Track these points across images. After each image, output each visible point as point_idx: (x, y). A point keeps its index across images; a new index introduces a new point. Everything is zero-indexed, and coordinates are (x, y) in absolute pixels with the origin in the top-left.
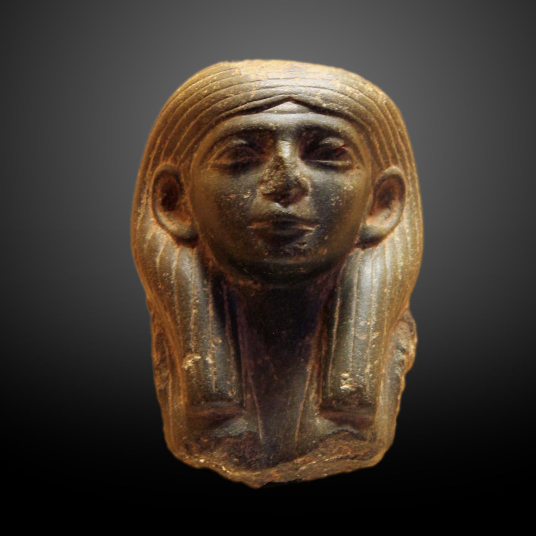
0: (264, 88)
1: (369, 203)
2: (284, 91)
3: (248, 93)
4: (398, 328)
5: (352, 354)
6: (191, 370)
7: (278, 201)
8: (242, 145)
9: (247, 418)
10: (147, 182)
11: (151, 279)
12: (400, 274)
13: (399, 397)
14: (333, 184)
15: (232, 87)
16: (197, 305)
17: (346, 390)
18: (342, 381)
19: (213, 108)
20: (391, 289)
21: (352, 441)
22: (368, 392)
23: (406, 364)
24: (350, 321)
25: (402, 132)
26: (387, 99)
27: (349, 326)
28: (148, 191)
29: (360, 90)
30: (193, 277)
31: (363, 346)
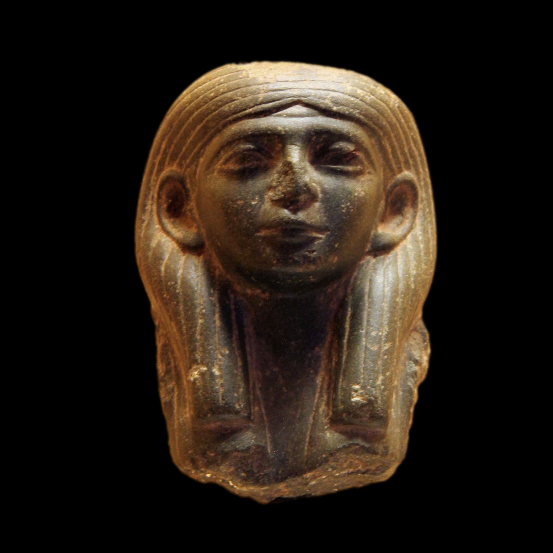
0: (273, 91)
1: (380, 209)
2: (293, 94)
3: (256, 96)
4: (411, 339)
5: (363, 366)
6: (197, 382)
7: (286, 207)
8: (249, 150)
9: (255, 432)
10: (152, 188)
11: (156, 288)
12: (413, 282)
13: (412, 410)
14: (344, 189)
15: (240, 90)
16: (203, 315)
17: (357, 403)
18: (353, 393)
19: (220, 112)
20: (403, 298)
21: (363, 455)
23: (418, 376)
24: (361, 331)
25: (415, 136)
27: (360, 337)
28: (153, 197)
29: (371, 93)
30: (199, 286)
31: (374, 357)
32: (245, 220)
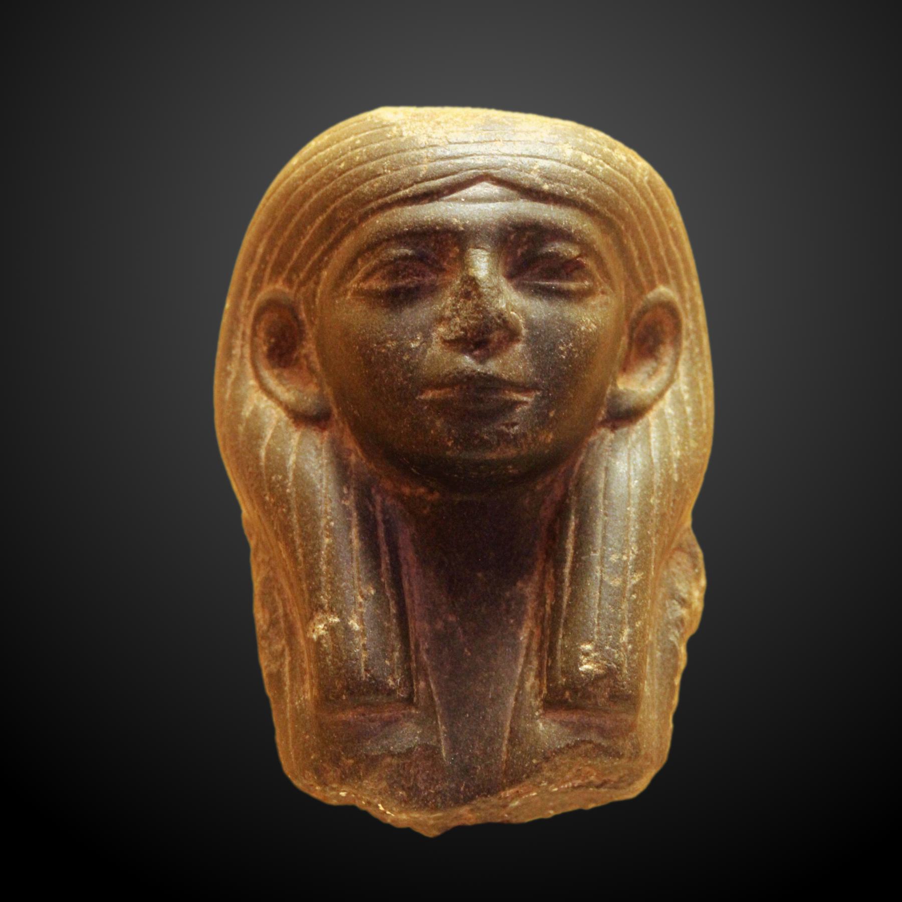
0: (442, 159)
1: (621, 352)
2: (476, 164)
3: (415, 168)
4: (673, 563)
5: (598, 612)
6: (323, 641)
7: (470, 352)
8: (405, 258)
9: (420, 723)
10: (243, 320)
11: (252, 485)
12: (675, 471)
13: (677, 681)
14: (562, 321)
15: (389, 157)
16: (331, 531)
17: (587, 673)
18: (582, 657)
19: (356, 194)
20: (661, 498)
21: (599, 759)
22: (626, 675)
23: (686, 624)
24: (592, 554)
25: (675, 229)
26: (650, 174)
28: (244, 334)
29: (604, 161)
30: (324, 482)
31: (616, 598)
32: (400, 374)
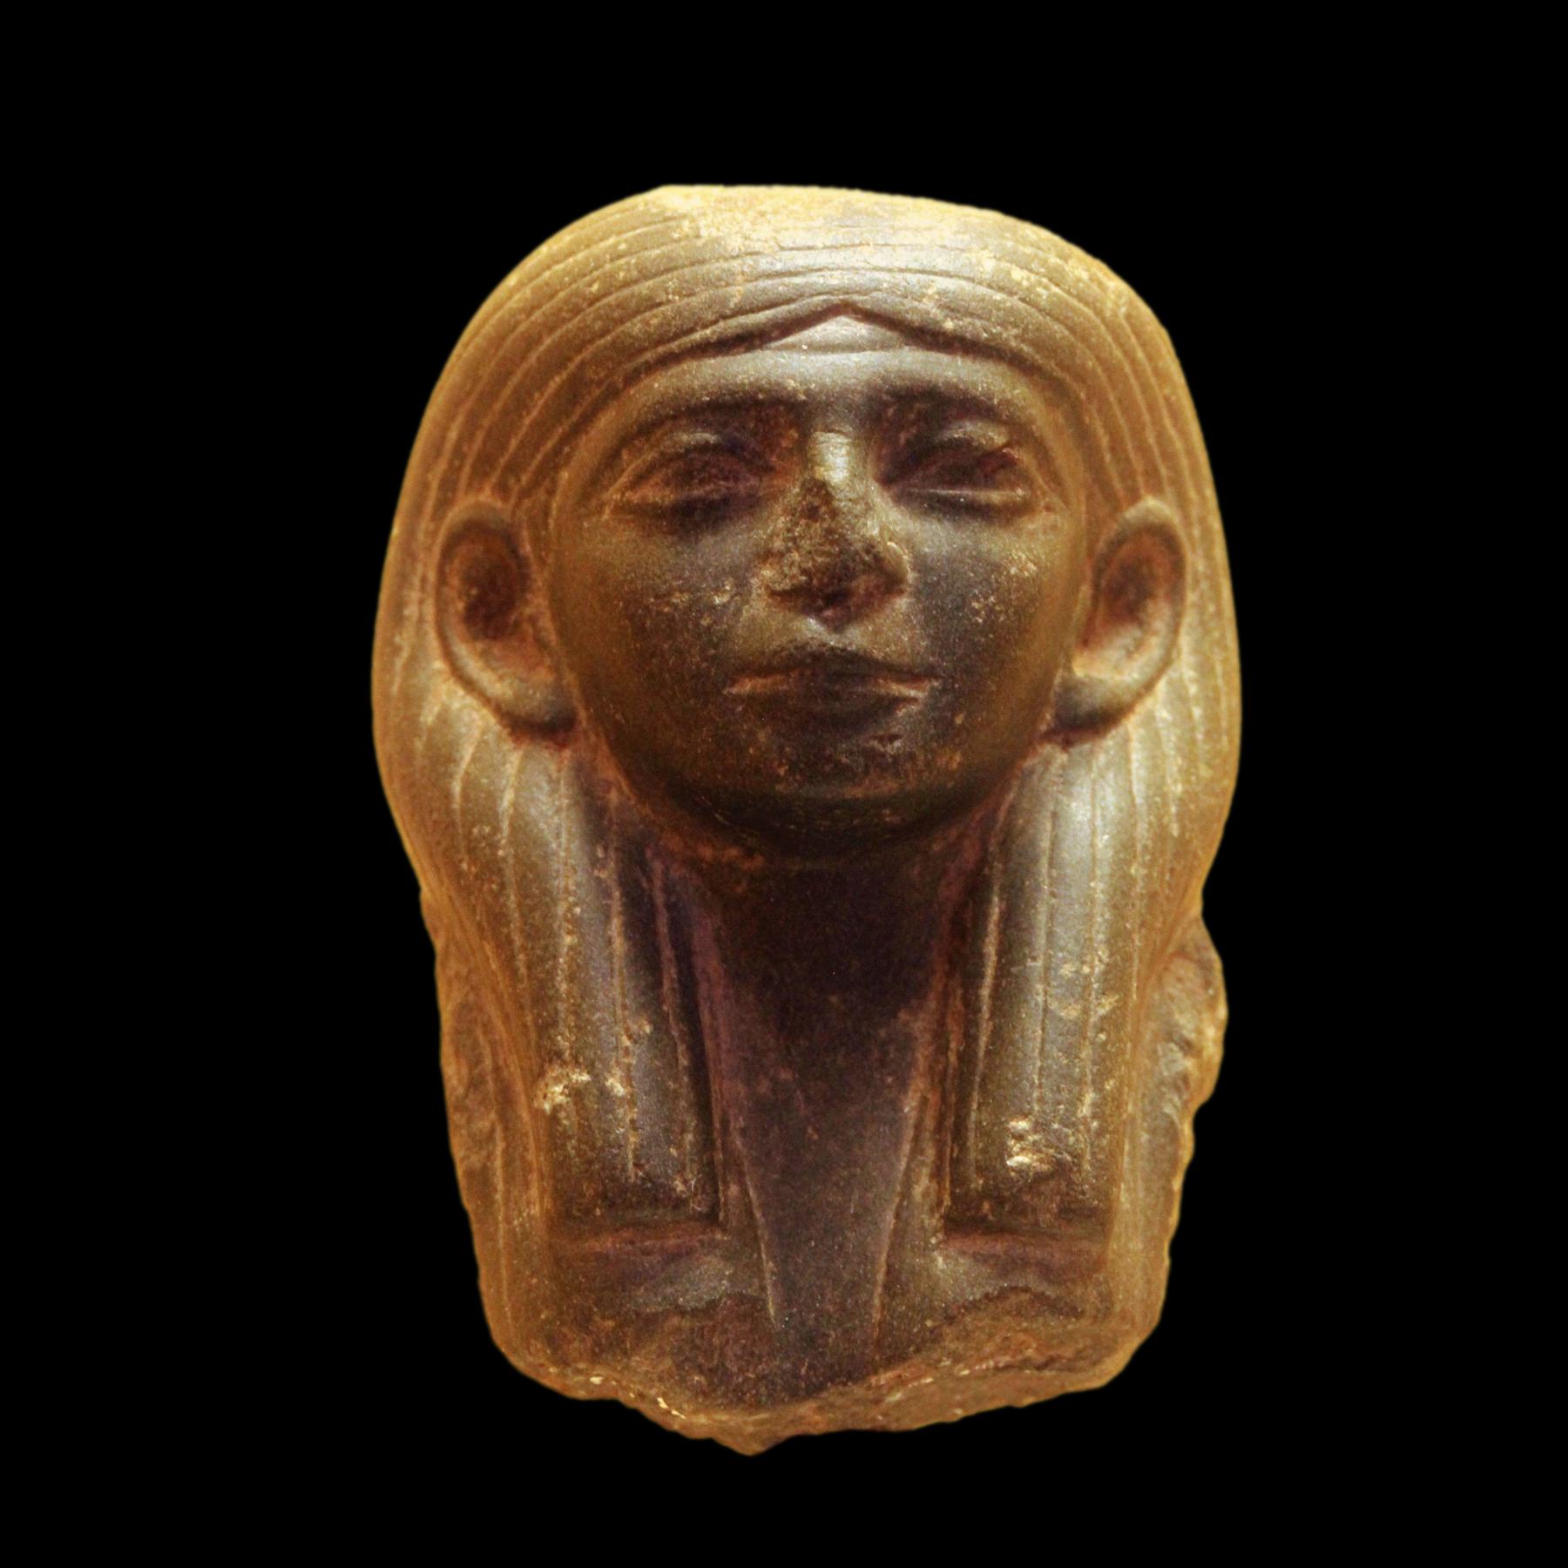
0: (769, 276)
1: (1079, 612)
2: (828, 286)
3: (721, 292)
4: (1169, 979)
5: (1039, 1064)
6: (562, 1115)
7: (817, 612)
8: (704, 448)
9: (730, 1257)
10: (422, 555)
11: (438, 843)
12: (1174, 819)
13: (1177, 1184)
14: (978, 558)
15: (675, 273)
16: (576, 922)
17: (1021, 1170)
18: (1011, 1142)
19: (618, 337)
20: (1150, 865)
21: (1041, 1320)
23: (1192, 1084)
24: (1030, 963)
25: (1173, 398)
26: (1130, 303)
27: (1027, 980)
28: (424, 580)
29: (1050, 280)
30: (564, 838)
31: (1071, 1039)
